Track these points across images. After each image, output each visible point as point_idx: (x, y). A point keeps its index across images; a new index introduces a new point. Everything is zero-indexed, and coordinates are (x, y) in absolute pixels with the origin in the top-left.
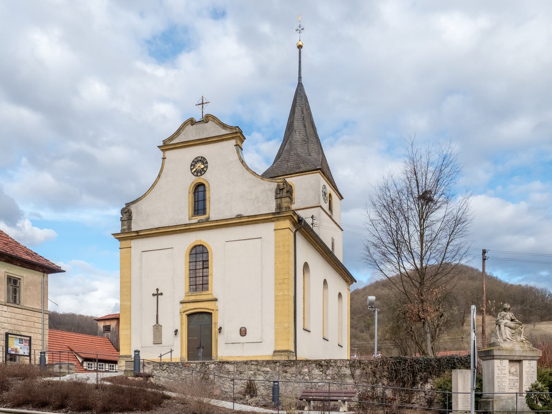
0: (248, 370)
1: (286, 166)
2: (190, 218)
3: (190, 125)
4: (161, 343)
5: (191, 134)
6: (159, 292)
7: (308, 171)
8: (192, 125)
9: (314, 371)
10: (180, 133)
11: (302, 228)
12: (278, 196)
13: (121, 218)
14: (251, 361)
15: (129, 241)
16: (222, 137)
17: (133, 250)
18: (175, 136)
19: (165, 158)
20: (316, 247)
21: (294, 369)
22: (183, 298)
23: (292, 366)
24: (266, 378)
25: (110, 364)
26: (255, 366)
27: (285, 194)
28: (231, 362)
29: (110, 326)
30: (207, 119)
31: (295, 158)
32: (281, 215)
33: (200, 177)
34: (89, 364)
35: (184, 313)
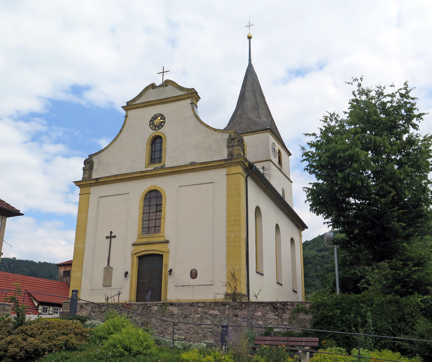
0: (194, 313)
1: (239, 127)
3: (151, 89)
4: (111, 286)
5: (152, 96)
6: (113, 235)
7: (259, 131)
8: (153, 89)
9: (268, 315)
11: (253, 174)
12: (230, 145)
13: (83, 167)
14: (198, 303)
15: (88, 188)
17: (91, 196)
19: (128, 116)
20: (268, 193)
21: (245, 312)
23: (244, 309)
24: (214, 322)
25: (54, 308)
26: (202, 308)
27: (236, 143)
28: (176, 303)
29: (70, 271)
31: (246, 121)
32: (233, 161)
33: (158, 131)
34: (55, 309)
35: (135, 255)
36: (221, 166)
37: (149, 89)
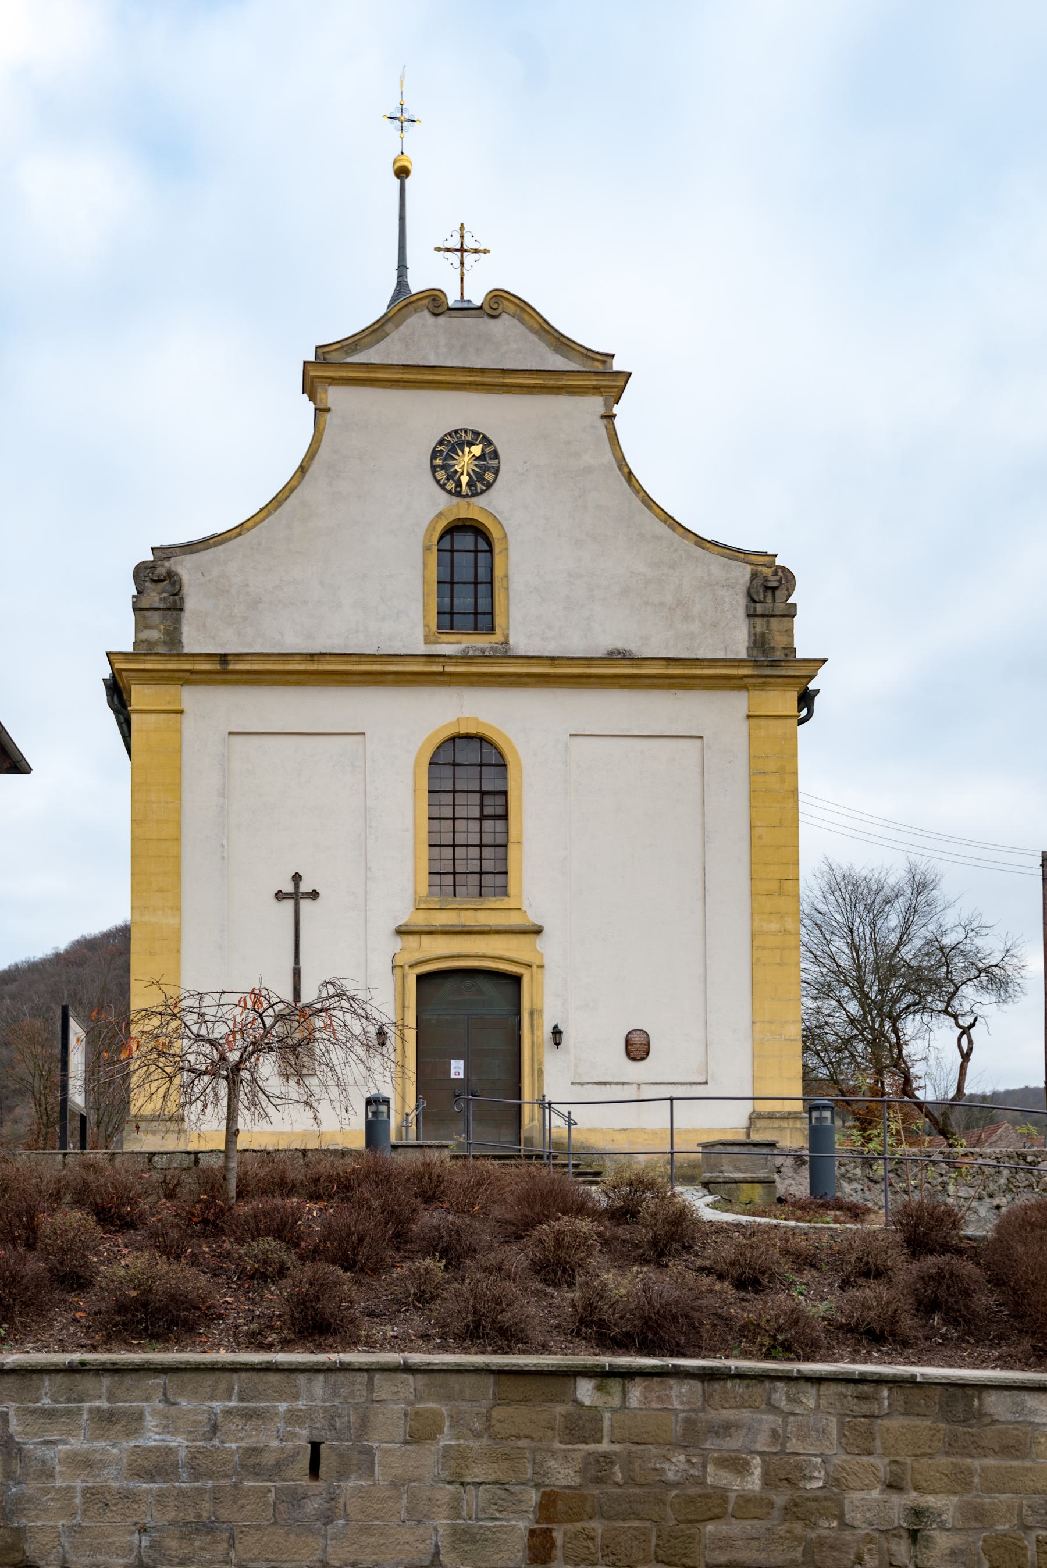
2: (432, 638)
3: (426, 313)
6: (305, 887)
8: (436, 315)
10: (388, 334)
12: (760, 608)
15: (172, 689)
16: (558, 380)
17: (188, 722)
18: (366, 340)
22: (405, 916)
30: (495, 306)
32: (783, 672)
33: (468, 499)
36: (733, 682)
37: (416, 311)
